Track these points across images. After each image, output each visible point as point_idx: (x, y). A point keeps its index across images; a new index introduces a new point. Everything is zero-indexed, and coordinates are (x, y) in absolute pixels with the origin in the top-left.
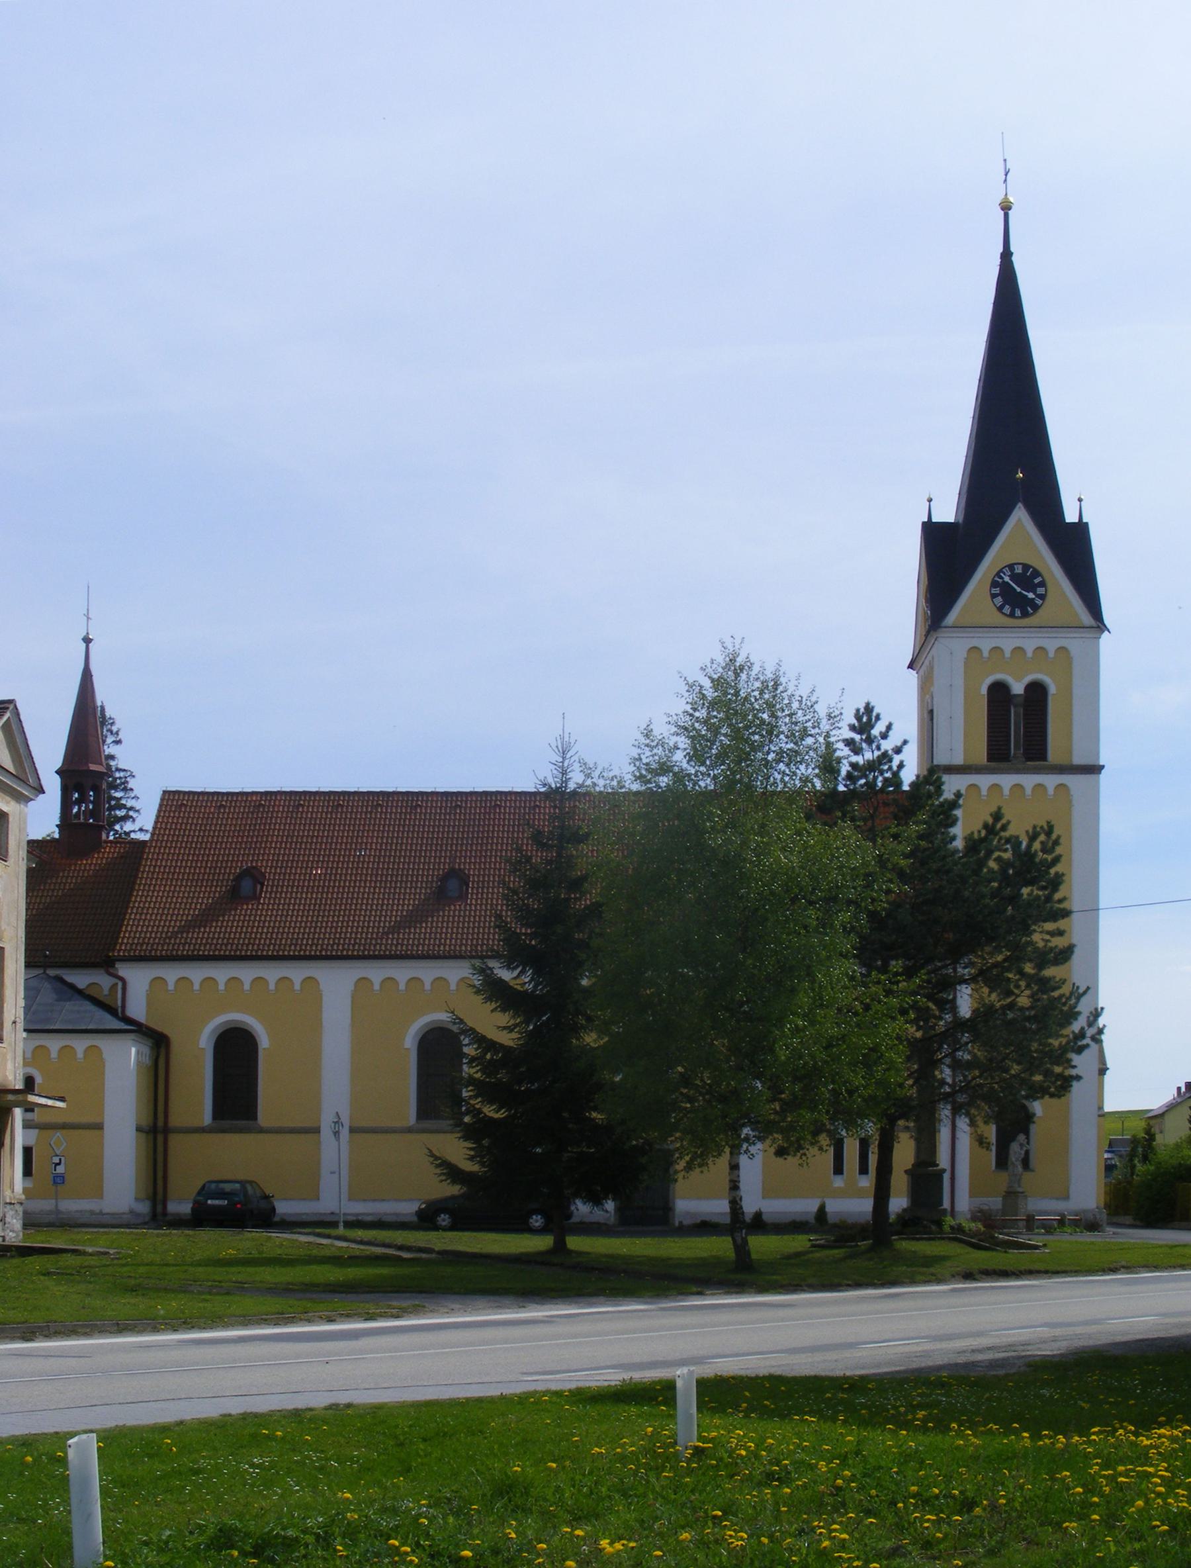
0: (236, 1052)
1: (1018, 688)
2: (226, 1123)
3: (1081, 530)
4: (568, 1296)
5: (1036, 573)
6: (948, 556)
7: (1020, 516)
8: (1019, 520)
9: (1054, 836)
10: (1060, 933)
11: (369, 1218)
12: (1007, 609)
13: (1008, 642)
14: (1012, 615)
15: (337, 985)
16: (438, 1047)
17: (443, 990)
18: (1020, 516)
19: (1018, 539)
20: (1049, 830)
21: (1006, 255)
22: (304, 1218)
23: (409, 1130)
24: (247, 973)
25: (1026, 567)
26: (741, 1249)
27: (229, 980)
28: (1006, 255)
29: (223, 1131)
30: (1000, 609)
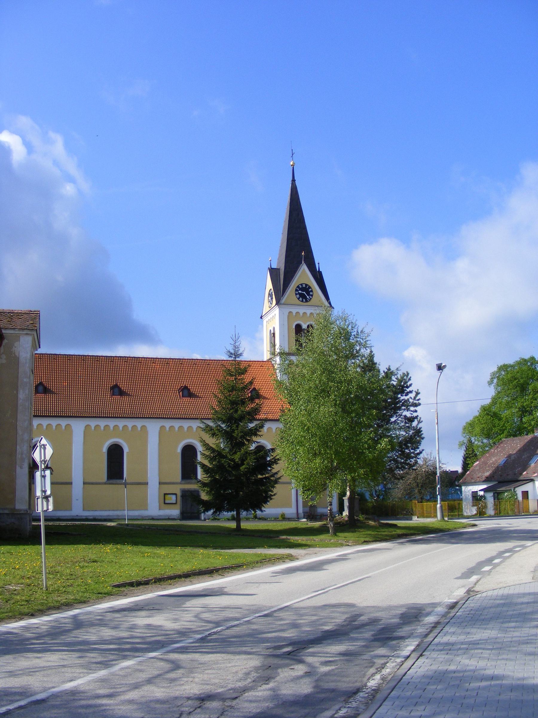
0: (115, 454)
1: (304, 326)
2: (111, 481)
3: (320, 273)
4: (168, 546)
5: (310, 287)
6: (282, 280)
7: (304, 268)
8: (304, 269)
9: (409, 377)
10: (416, 411)
11: (91, 518)
12: (301, 299)
13: (302, 310)
14: (302, 301)
15: (153, 428)
16: (189, 452)
17: (193, 433)
18: (304, 268)
19: (303, 275)
20: (408, 374)
21: (294, 180)
22: (54, 518)
23: (105, 483)
24: (121, 423)
25: (306, 285)
26: (238, 525)
27: (161, 427)
28: (294, 180)
29: (110, 484)
30: (299, 299)
